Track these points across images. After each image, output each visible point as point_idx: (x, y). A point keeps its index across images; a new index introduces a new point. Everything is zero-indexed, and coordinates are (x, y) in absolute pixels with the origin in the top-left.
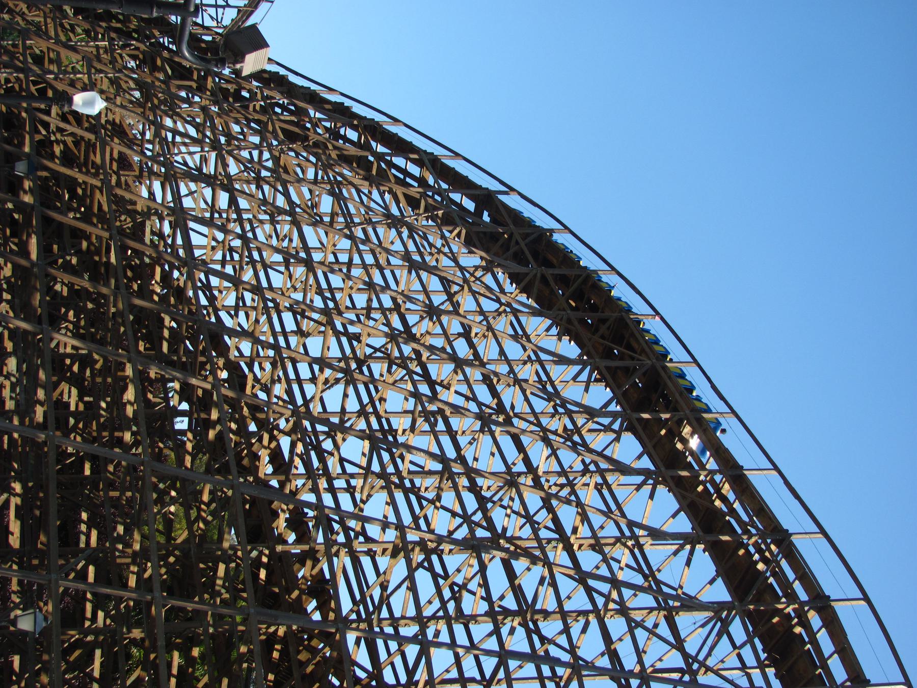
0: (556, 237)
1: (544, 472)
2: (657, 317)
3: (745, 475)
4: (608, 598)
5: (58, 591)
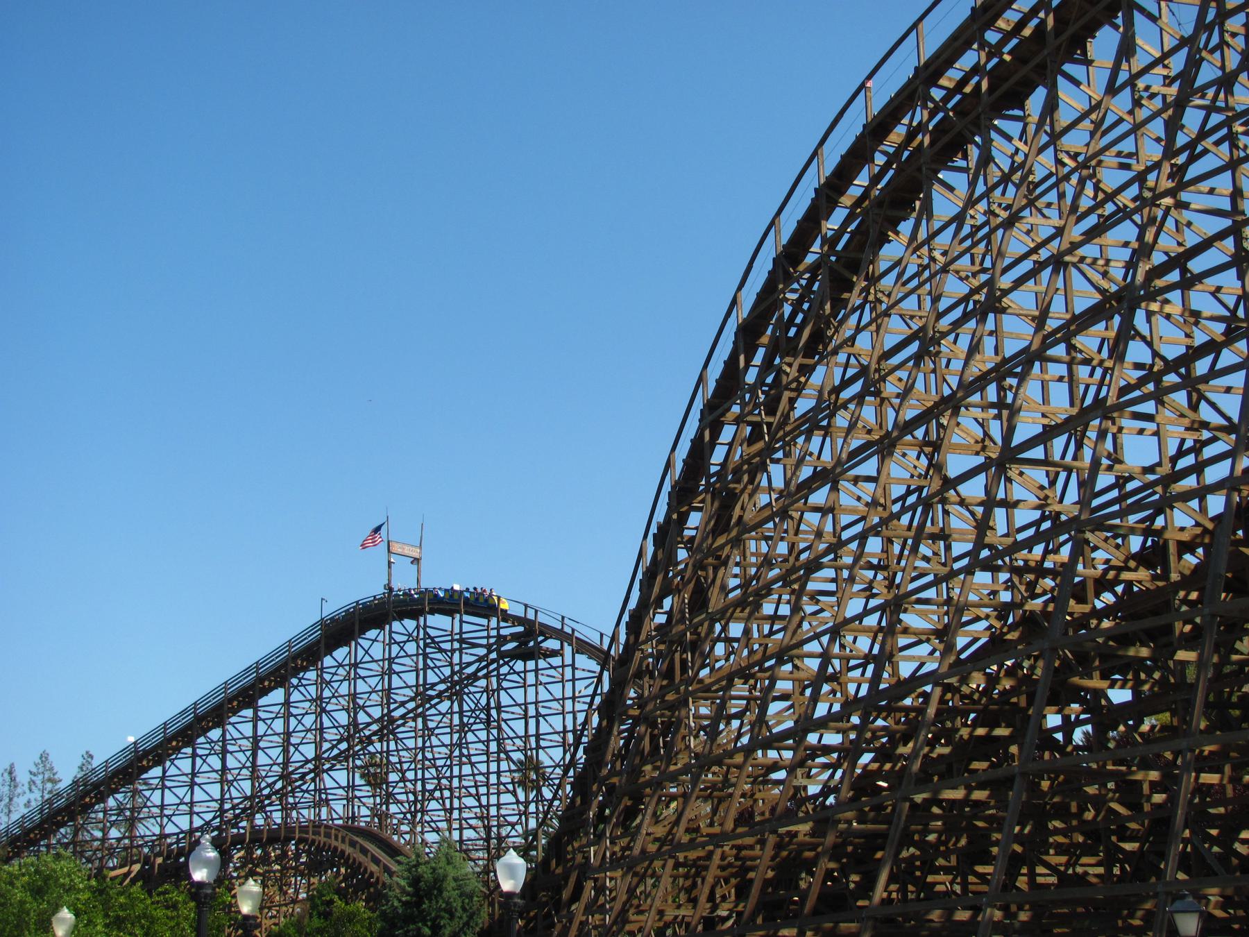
0: (785, 239)
1: (1060, 218)
2: (868, 85)
3: (925, 63)
4: (1210, 109)
5: (1184, 881)
